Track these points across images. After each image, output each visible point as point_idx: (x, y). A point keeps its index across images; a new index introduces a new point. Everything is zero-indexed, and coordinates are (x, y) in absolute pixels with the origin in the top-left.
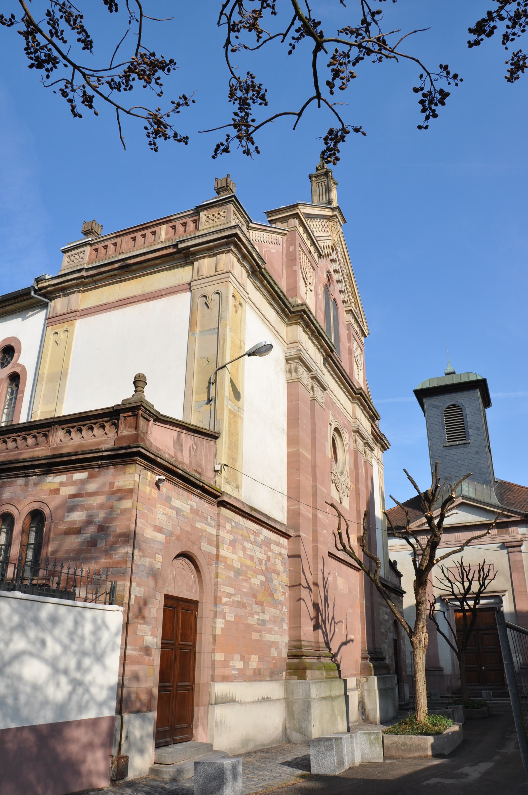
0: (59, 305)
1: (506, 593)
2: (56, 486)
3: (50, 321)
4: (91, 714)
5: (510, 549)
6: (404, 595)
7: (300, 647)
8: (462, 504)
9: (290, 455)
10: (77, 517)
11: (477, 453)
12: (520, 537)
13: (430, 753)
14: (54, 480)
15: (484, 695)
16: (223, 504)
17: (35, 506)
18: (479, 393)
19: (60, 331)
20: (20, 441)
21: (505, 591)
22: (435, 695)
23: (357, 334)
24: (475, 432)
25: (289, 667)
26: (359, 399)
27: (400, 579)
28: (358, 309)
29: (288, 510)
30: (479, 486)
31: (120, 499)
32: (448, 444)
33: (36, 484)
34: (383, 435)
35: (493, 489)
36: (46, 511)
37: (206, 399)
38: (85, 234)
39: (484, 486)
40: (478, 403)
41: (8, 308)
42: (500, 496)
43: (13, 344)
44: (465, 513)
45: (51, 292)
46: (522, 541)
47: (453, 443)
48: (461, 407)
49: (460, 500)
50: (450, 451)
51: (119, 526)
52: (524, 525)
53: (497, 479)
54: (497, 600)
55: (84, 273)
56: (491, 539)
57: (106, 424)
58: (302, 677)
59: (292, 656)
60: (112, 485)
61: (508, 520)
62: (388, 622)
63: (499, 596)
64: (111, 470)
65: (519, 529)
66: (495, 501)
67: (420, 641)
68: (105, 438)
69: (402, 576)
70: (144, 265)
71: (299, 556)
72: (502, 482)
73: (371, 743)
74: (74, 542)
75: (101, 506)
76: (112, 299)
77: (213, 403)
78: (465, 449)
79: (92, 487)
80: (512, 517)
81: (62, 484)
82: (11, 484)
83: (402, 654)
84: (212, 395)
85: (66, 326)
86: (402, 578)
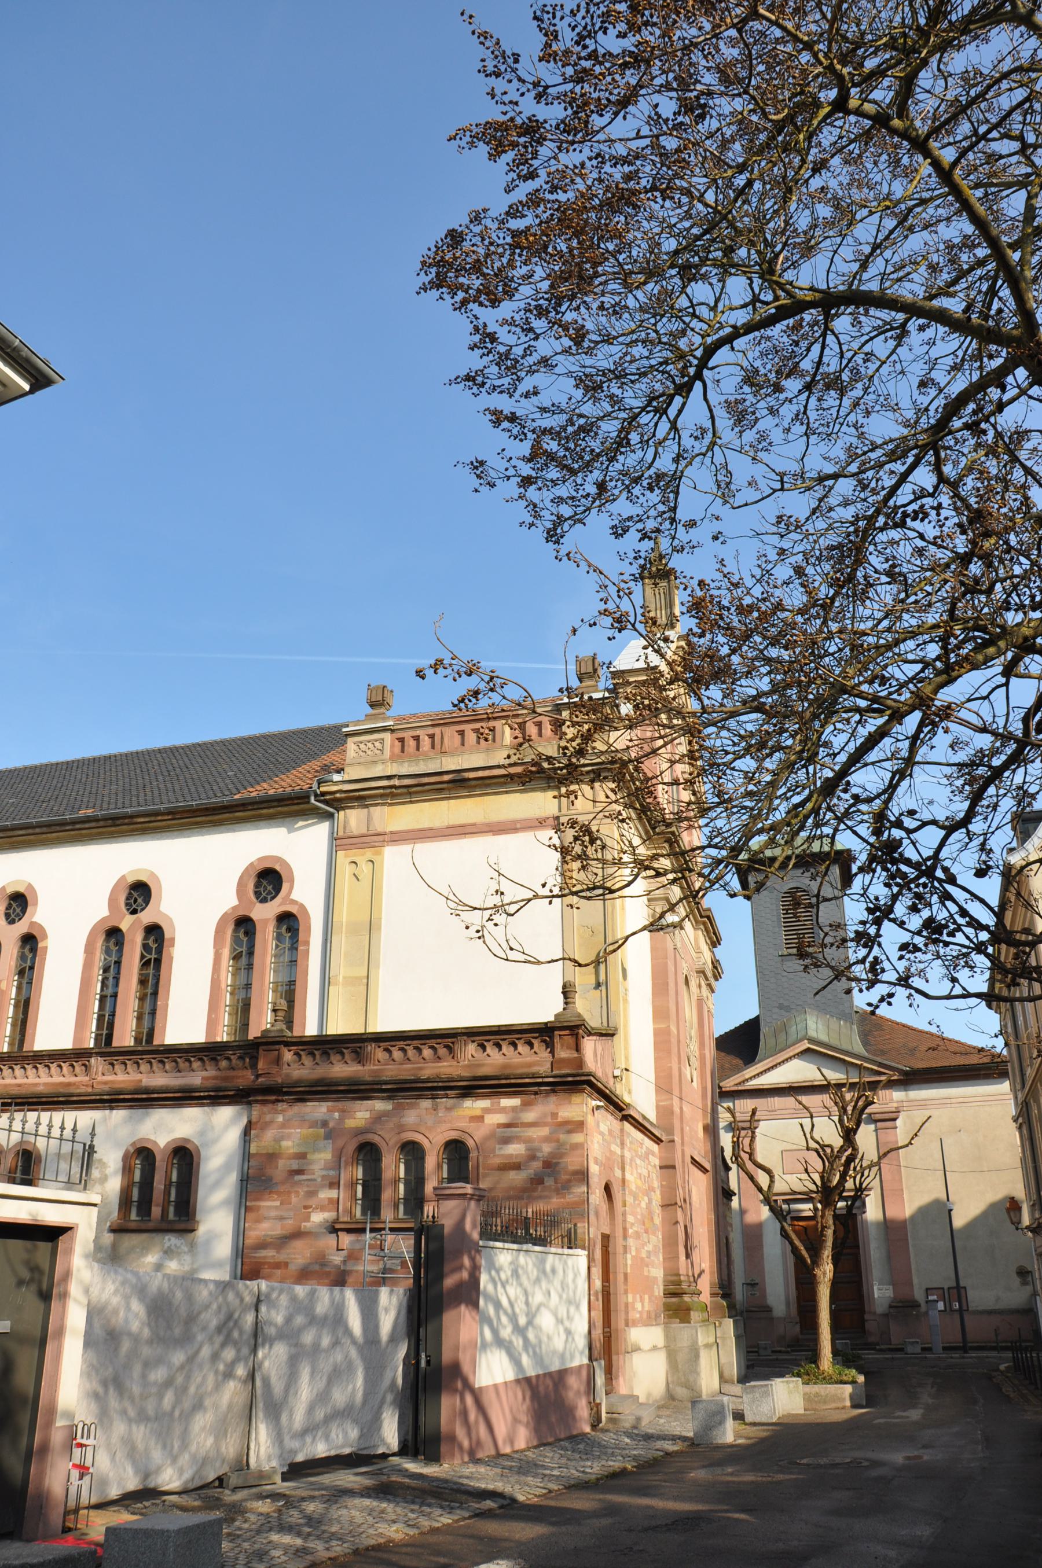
0: (353, 819)
2: (478, 1113)
3: (338, 842)
4: (576, 1363)
7: (679, 1283)
9: (657, 1033)
10: (515, 1150)
13: (848, 1403)
14: (475, 1106)
16: (626, 1118)
17: (453, 1135)
19: (361, 860)
20: (411, 1052)
25: (667, 1307)
26: (704, 924)
29: (657, 1107)
30: (834, 1023)
31: (570, 1132)
33: (449, 1109)
35: (855, 1027)
36: (470, 1143)
37: (593, 981)
38: (371, 706)
41: (265, 811)
43: (278, 868)
45: (340, 800)
49: (806, 1045)
51: (571, 1162)
55: (396, 782)
57: (536, 1042)
58: (685, 1319)
59: (669, 1294)
60: (554, 1115)
61: (877, 1078)
64: (553, 1099)
66: (859, 1048)
67: (824, 1274)
68: (535, 1058)
70: (488, 782)
71: (674, 1167)
73: (790, 1392)
74: (516, 1178)
75: (546, 1139)
76: (437, 823)
77: (603, 988)
79: (530, 1116)
81: (486, 1111)
82: (412, 1106)
84: (602, 978)
85: (369, 854)
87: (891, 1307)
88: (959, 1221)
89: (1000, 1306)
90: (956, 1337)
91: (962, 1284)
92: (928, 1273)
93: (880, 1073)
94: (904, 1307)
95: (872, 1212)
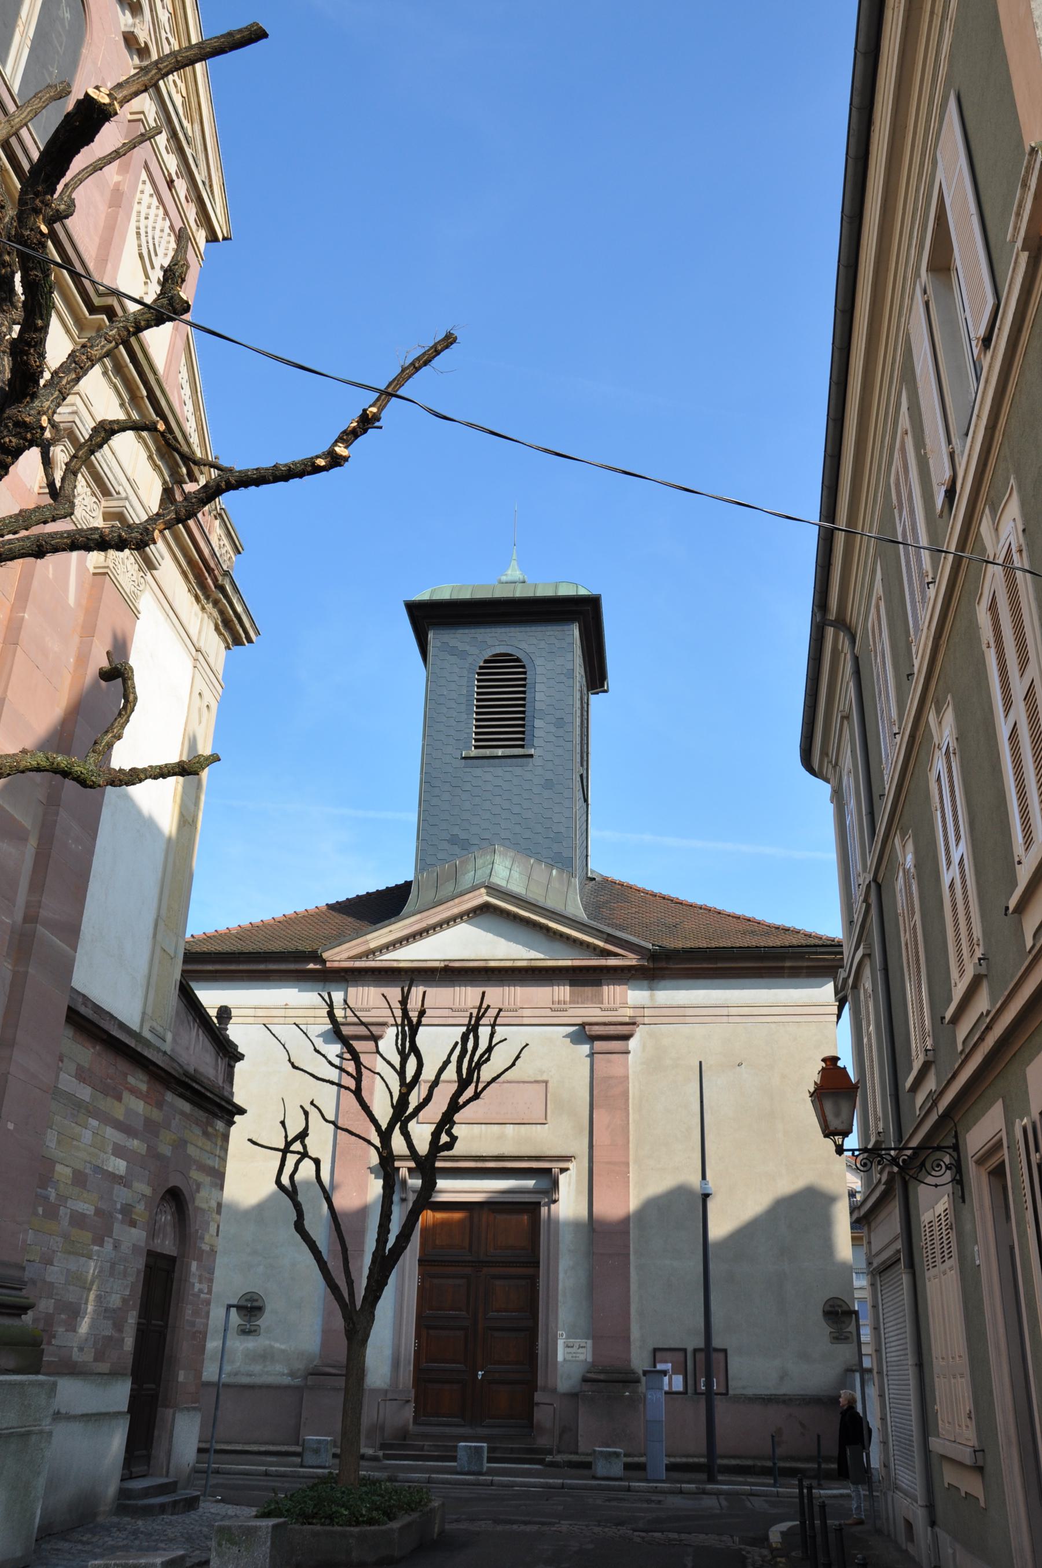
1: (570, 1165)
5: (599, 1045)
6: (237, 1118)
8: (484, 910)
11: (548, 784)
12: (629, 1012)
15: (461, 1454)
18: (577, 633)
21: (568, 1158)
22: (317, 1451)
23: (170, 184)
24: (553, 729)
27: (232, 1067)
28: (197, 127)
30: (540, 872)
32: (474, 752)
34: (226, 574)
39: (554, 872)
40: (569, 656)
42: (594, 908)
44: (490, 936)
46: (634, 1024)
47: (488, 752)
48: (525, 662)
49: (482, 897)
50: (478, 772)
52: (646, 983)
53: (593, 871)
54: (545, 1184)
56: (549, 1012)
62: (127, 1185)
63: (550, 1170)
65: (630, 992)
66: (576, 909)
69: (240, 1057)
72: (606, 880)
78: (518, 771)
80: (616, 955)
83: (188, 1311)
86: (239, 1066)
87: (585, 1380)
88: (719, 1228)
89: (787, 1389)
90: (694, 1447)
91: (717, 1342)
92: (659, 1317)
93: (606, 954)
94: (611, 1383)
95: (568, 1204)
